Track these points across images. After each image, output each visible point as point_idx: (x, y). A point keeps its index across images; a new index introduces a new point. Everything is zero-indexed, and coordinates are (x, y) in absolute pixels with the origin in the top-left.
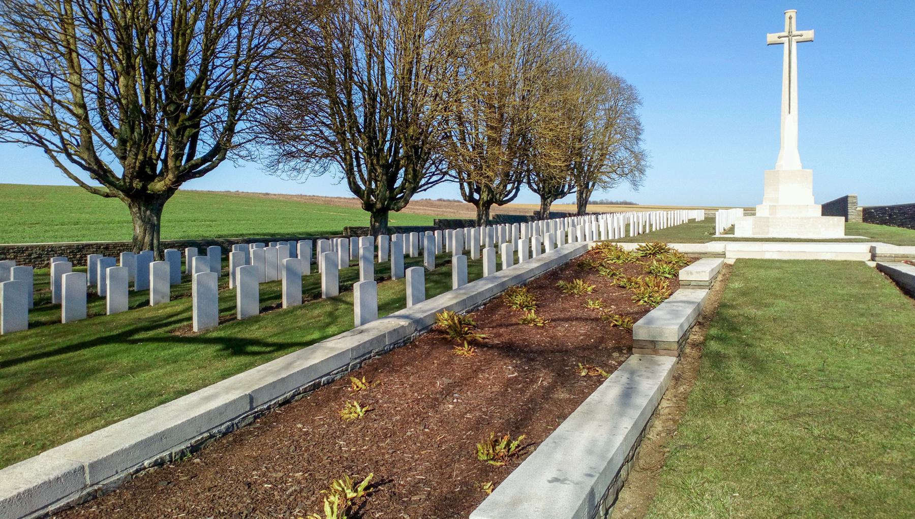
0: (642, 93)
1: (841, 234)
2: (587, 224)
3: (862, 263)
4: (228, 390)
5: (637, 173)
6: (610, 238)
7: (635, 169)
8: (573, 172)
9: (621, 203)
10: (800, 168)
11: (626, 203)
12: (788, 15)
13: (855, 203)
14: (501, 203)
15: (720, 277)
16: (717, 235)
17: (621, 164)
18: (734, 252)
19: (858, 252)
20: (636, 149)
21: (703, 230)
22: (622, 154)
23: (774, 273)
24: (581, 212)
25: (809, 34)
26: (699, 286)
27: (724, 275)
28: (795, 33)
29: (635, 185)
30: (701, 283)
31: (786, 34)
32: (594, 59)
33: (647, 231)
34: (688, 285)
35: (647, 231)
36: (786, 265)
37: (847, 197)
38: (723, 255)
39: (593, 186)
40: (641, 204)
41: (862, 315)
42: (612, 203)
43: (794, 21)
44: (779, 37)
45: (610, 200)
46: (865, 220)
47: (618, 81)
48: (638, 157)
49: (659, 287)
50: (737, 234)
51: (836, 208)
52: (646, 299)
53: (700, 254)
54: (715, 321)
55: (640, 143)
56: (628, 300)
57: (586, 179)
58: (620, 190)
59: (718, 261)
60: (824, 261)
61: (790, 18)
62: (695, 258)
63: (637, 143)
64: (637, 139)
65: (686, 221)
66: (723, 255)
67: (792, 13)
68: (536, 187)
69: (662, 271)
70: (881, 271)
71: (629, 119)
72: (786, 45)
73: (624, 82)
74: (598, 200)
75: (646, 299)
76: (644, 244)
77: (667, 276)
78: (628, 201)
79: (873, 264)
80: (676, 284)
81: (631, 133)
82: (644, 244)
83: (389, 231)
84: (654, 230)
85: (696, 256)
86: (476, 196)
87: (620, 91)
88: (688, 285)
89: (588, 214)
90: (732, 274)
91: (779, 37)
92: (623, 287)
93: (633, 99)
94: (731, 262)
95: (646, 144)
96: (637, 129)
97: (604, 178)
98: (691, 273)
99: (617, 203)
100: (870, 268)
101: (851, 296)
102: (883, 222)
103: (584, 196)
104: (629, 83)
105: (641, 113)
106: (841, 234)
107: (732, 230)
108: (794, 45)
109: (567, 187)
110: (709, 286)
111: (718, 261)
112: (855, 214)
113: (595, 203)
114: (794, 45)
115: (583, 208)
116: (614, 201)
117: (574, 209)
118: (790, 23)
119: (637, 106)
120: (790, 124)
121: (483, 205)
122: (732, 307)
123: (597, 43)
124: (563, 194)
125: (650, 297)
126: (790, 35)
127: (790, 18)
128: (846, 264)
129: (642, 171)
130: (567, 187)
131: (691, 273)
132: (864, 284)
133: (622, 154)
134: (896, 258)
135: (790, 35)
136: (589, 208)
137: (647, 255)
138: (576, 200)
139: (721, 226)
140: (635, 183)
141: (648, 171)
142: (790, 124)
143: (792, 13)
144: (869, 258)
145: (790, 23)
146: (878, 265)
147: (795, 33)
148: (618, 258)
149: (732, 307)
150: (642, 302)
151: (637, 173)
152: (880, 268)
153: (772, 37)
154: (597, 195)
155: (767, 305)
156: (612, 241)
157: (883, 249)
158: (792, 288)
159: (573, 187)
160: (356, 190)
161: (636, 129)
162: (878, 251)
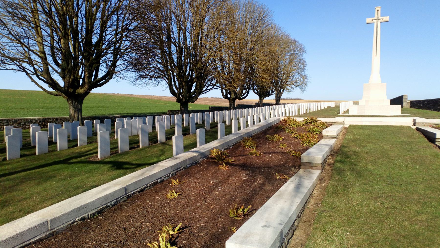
0: (306, 47)
1: (399, 113)
3: (409, 127)
4: (115, 185)
5: (303, 85)
7: (303, 83)
8: (273, 84)
9: (296, 99)
11: (298, 99)
12: (377, 9)
13: (406, 99)
14: (240, 99)
15: (342, 134)
17: (296, 81)
18: (349, 122)
19: (407, 122)
20: (303, 74)
21: (334, 111)
23: (367, 132)
24: (277, 103)
25: (386, 18)
26: (332, 137)
27: (343, 132)
28: (380, 18)
29: (302, 90)
31: (375, 18)
32: (284, 31)
33: (308, 112)
34: (327, 137)
35: (308, 112)
38: (343, 123)
39: (283, 91)
40: (305, 99)
41: (409, 151)
42: (292, 99)
44: (372, 20)
45: (291, 98)
46: (411, 106)
48: (304, 77)
50: (350, 113)
55: (305, 71)
57: (279, 89)
59: (341, 126)
60: (391, 126)
61: (378, 11)
62: (330, 125)
64: (304, 69)
65: (326, 107)
66: (343, 123)
67: (379, 8)
68: (256, 92)
70: (418, 131)
71: (300, 59)
72: (375, 24)
73: (298, 42)
74: (285, 98)
76: (306, 118)
78: (299, 98)
79: (414, 127)
81: (301, 66)
82: (306, 118)
83: (189, 112)
84: (311, 111)
85: (331, 123)
86: (229, 96)
88: (327, 137)
89: (281, 104)
91: (372, 20)
92: (297, 138)
93: (302, 50)
95: (308, 71)
96: (304, 64)
97: (288, 87)
98: (328, 131)
100: (413, 129)
101: (403, 142)
102: (420, 108)
104: (300, 42)
105: (306, 57)
107: (348, 111)
109: (271, 91)
111: (341, 126)
112: (406, 104)
113: (284, 99)
114: (379, 24)
116: (293, 98)
117: (274, 102)
118: (378, 13)
120: (376, 61)
121: (232, 100)
123: (286, 23)
124: (269, 95)
127: (378, 11)
128: (401, 127)
129: (306, 84)
130: (271, 91)
131: (328, 131)
132: (409, 137)
133: (297, 76)
136: (281, 101)
138: (275, 98)
139: (342, 110)
140: (302, 90)
141: (309, 84)
142: (376, 61)
143: (379, 8)
144: (413, 123)
145: (378, 13)
147: (380, 18)
149: (347, 147)
150: (305, 145)
152: (418, 129)
153: (369, 20)
154: (285, 95)
159: (274, 92)
160: (172, 92)
161: (303, 64)
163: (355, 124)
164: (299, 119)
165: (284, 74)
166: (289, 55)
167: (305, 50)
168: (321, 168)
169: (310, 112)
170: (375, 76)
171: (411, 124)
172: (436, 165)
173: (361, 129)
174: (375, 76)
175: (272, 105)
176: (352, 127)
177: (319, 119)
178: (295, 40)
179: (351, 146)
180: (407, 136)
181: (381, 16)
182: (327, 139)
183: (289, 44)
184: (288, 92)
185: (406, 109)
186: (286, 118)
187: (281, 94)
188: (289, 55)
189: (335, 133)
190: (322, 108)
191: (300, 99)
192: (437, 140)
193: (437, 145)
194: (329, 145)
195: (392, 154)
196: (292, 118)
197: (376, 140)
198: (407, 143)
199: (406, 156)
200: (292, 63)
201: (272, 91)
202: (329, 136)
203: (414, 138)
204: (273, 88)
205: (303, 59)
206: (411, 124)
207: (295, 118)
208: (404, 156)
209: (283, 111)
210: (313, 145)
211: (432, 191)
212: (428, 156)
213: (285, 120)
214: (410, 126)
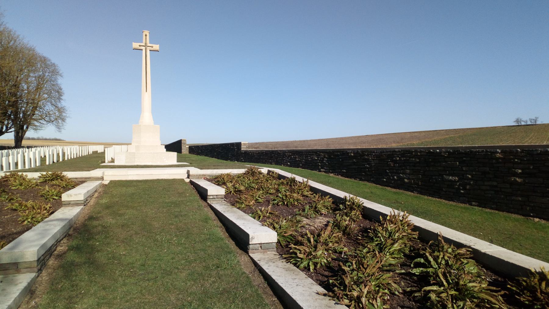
1: (175, 162)
2: (16, 155)
3: (183, 180)
5: (60, 121)
6: (27, 167)
7: (59, 118)
9: (53, 140)
10: (153, 124)
11: (56, 140)
12: (144, 34)
15: (96, 195)
16: (106, 164)
17: (48, 114)
18: (110, 175)
19: (180, 173)
20: (59, 105)
21: (95, 160)
22: (49, 107)
23: (131, 190)
24: (18, 144)
25: (156, 47)
26: (76, 204)
27: (100, 193)
28: (149, 45)
29: (59, 128)
30: (79, 202)
31: (144, 44)
32: (25, 41)
33: (61, 160)
34: (69, 204)
35: (61, 160)
36: (139, 184)
37: (181, 140)
38: (102, 179)
39: (27, 128)
40: (67, 140)
41: (176, 217)
42: (46, 139)
43: (148, 37)
44: (140, 46)
45: (44, 137)
46: (190, 152)
47: (44, 60)
48: (61, 110)
49: (41, 209)
50: (116, 163)
51: (175, 147)
52: (29, 220)
53: (86, 178)
54: (80, 233)
55: (62, 101)
56: (16, 221)
58: (48, 131)
59: (97, 183)
60: (162, 180)
61: (146, 35)
62: (82, 181)
63: (60, 102)
65: (91, 152)
66: (102, 179)
67: (146, 32)
69: (51, 194)
70: (192, 184)
71: (53, 85)
72: (144, 51)
73: (49, 60)
74: (31, 137)
75: (29, 220)
76: (44, 173)
77: (55, 197)
78: (58, 138)
79: (188, 180)
80: (59, 204)
81: (54, 94)
82: (44, 173)
84: (66, 159)
85: (83, 180)
87: (47, 66)
88: (69, 204)
89: (23, 147)
90: (105, 192)
91: (140, 46)
92: (15, 210)
93: (55, 72)
94: (106, 182)
95: (66, 102)
96: (59, 93)
97: (36, 123)
98: (71, 196)
99: (50, 139)
100: (186, 183)
101: (172, 203)
102: (198, 154)
103: (20, 135)
104: (53, 62)
105: (61, 82)
106: (175, 162)
107: (113, 161)
108: (148, 52)
109: (4, 128)
110: (85, 203)
111: (97, 183)
112: (185, 150)
113: (29, 139)
114: (148, 52)
115: (19, 143)
116: (48, 138)
117: (13, 143)
118: (146, 38)
119: (59, 77)
120: (147, 98)
122: (97, 219)
125: (33, 218)
126: (146, 46)
127: (146, 35)
128: (174, 181)
129: (63, 120)
130: (4, 128)
131: (71, 196)
132: (180, 194)
133: (49, 107)
134: (199, 177)
135: (146, 46)
136: (24, 143)
137: (45, 181)
138: (13, 138)
139: (108, 158)
140: (59, 128)
141: (68, 120)
142: (147, 98)
143: (146, 32)
144: (187, 176)
145: (146, 38)
146: (191, 181)
147: (149, 45)
148: (21, 185)
149: (97, 219)
150: (26, 222)
151: (60, 121)
152: (192, 183)
153: (136, 45)
154: (30, 133)
155: (121, 215)
156: (20, 171)
157: (194, 171)
158: (139, 201)
159: (10, 128)
161: (58, 92)
162: (191, 173)
163: (117, 179)
164: (31, 175)
165: (27, 103)
166: (35, 77)
167: (61, 72)
168: (36, 270)
169: (64, 160)
170: (147, 117)
171: (184, 177)
172: (204, 234)
173: (124, 186)
174: (147, 117)
175: (9, 148)
176: (114, 183)
177: (64, 173)
178: (44, 58)
179: (102, 217)
180: (179, 193)
181: (150, 43)
182: (70, 208)
183: (32, 60)
184: (36, 129)
185: (185, 155)
186: (8, 174)
187: (24, 132)
188: (35, 77)
189: (81, 198)
190: (85, 153)
191: (59, 140)
192: (209, 197)
193: (208, 203)
194: (66, 219)
195: (156, 224)
196: (20, 173)
197: (139, 203)
198: (176, 204)
199: (172, 224)
200: (41, 88)
201: (7, 127)
202: (72, 203)
203: (186, 196)
204: (8, 124)
205: (57, 84)
206: (184, 177)
207: (24, 174)
208: (170, 224)
209: (51, 153)
210: (39, 222)
211: (195, 281)
212: (197, 220)
213: (6, 177)
214: (183, 180)
